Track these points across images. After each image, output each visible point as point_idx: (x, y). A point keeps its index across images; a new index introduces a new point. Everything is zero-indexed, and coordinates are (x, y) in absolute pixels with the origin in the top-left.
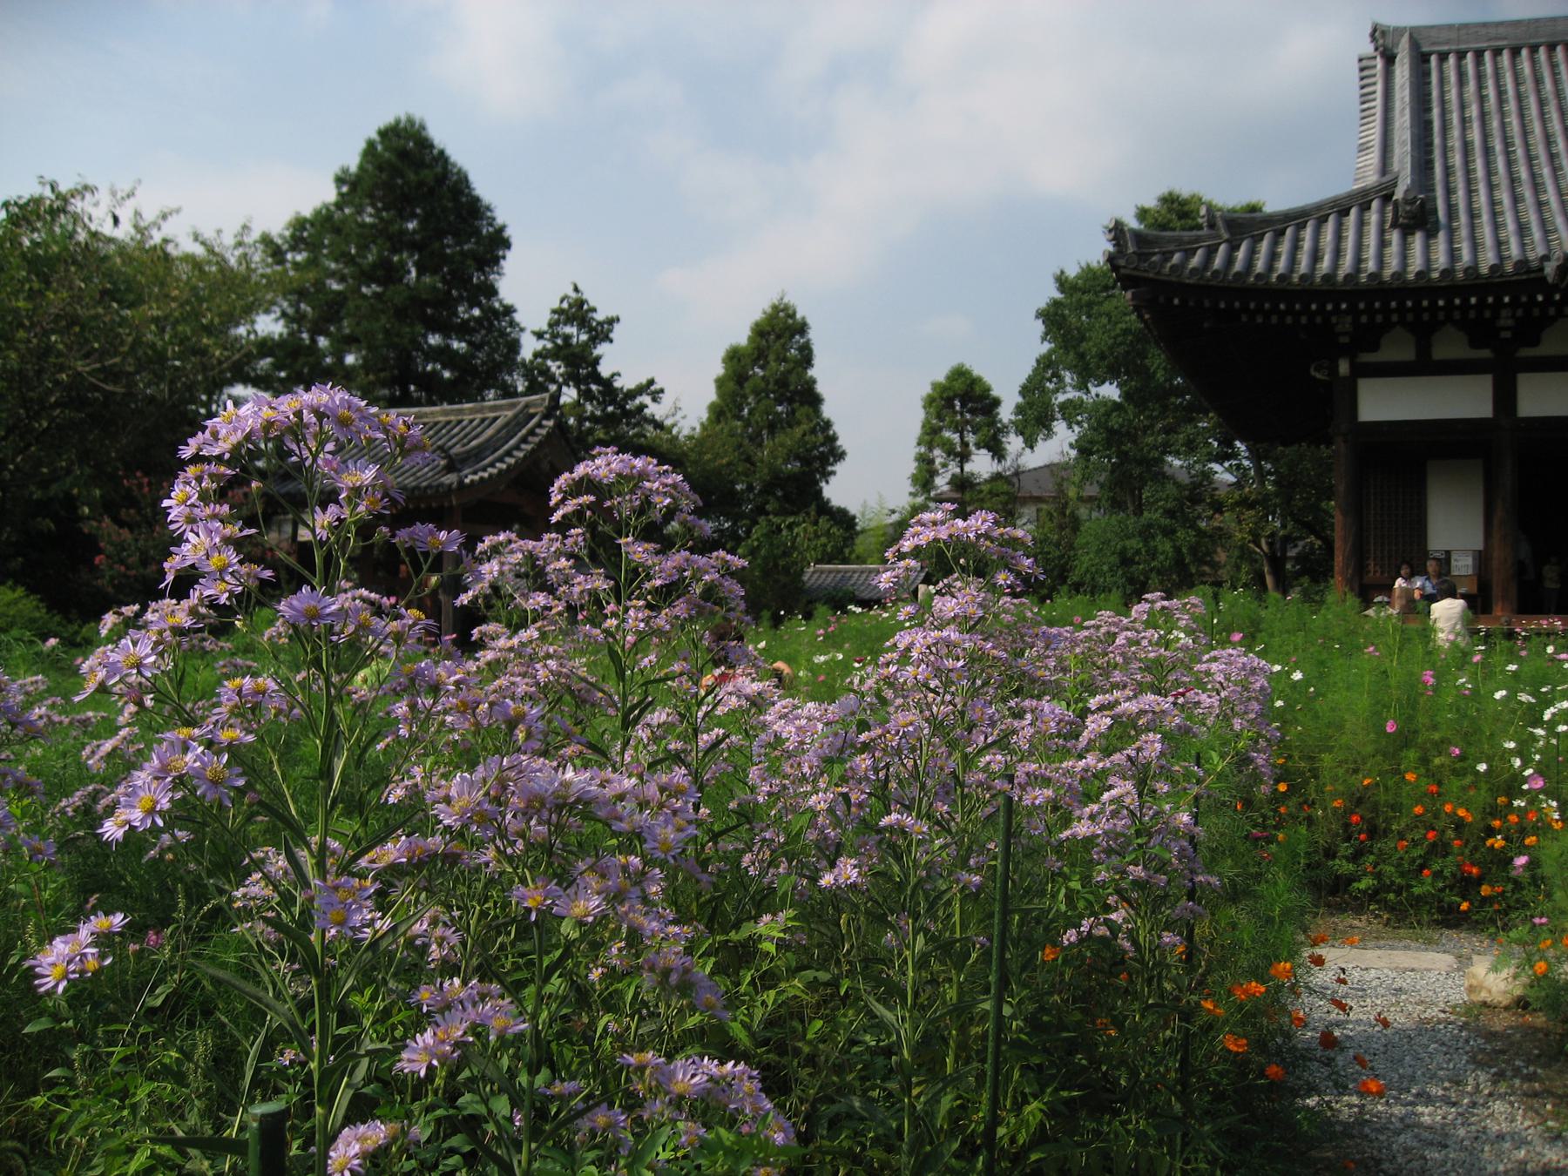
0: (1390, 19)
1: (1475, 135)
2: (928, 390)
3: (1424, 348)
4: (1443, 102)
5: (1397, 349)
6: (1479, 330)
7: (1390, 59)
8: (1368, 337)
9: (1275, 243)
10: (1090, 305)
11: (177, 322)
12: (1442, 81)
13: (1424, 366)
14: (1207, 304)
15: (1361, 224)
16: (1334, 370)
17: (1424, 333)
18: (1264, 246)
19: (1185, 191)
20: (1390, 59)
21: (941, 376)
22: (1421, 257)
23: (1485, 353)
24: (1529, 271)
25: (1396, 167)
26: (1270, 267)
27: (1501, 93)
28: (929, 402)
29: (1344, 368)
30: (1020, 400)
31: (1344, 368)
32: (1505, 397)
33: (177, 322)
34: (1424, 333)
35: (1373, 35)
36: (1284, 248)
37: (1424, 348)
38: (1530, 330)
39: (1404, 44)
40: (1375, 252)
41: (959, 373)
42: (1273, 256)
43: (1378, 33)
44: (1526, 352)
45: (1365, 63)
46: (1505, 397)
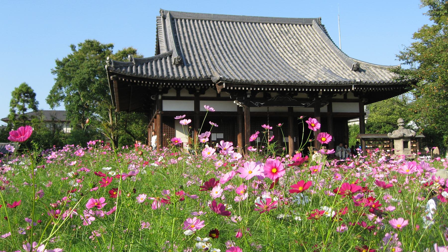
0: (165, 9)
1: (187, 41)
2: (14, 90)
3: (178, 93)
4: (179, 32)
5: (172, 93)
6: (192, 90)
7: (164, 18)
8: (165, 90)
9: (147, 66)
10: (74, 71)
11: (122, 176)
12: (178, 25)
13: (178, 98)
14: (131, 81)
15: (166, 62)
16: (157, 98)
17: (178, 90)
18: (144, 67)
19: (92, 39)
20: (164, 18)
21: (18, 86)
22: (182, 73)
23: (193, 95)
24: (208, 78)
25: (171, 49)
26: (147, 73)
27: (192, 31)
28: (14, 94)
29: (160, 97)
30: (50, 94)
31: (160, 97)
32: (197, 106)
33: (122, 176)
34: (178, 90)
35: (160, 12)
36: (149, 67)
37: (178, 93)
38: (203, 91)
39: (168, 15)
40: (168, 70)
41: (24, 86)
42: (147, 70)
43: (162, 11)
44: (202, 96)
45: (158, 19)
46: (197, 106)
